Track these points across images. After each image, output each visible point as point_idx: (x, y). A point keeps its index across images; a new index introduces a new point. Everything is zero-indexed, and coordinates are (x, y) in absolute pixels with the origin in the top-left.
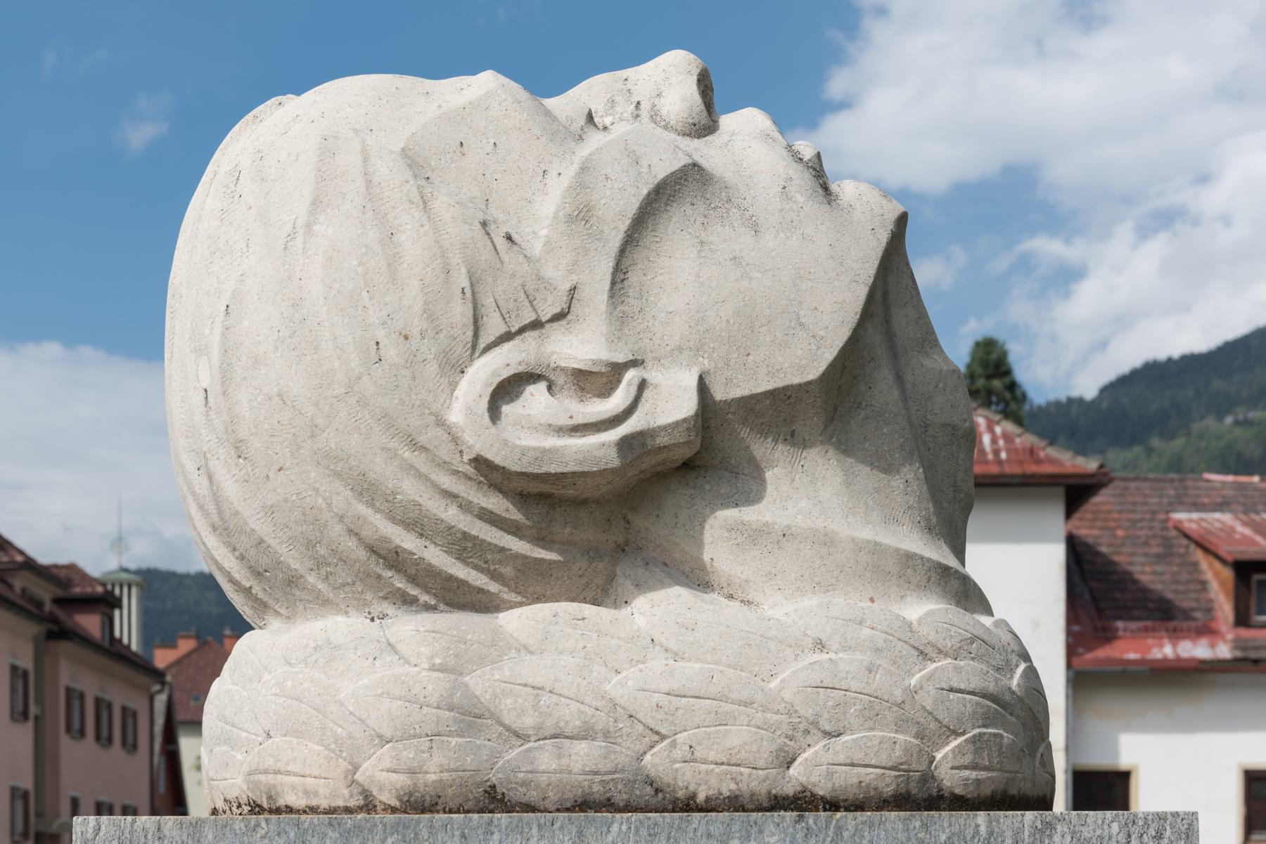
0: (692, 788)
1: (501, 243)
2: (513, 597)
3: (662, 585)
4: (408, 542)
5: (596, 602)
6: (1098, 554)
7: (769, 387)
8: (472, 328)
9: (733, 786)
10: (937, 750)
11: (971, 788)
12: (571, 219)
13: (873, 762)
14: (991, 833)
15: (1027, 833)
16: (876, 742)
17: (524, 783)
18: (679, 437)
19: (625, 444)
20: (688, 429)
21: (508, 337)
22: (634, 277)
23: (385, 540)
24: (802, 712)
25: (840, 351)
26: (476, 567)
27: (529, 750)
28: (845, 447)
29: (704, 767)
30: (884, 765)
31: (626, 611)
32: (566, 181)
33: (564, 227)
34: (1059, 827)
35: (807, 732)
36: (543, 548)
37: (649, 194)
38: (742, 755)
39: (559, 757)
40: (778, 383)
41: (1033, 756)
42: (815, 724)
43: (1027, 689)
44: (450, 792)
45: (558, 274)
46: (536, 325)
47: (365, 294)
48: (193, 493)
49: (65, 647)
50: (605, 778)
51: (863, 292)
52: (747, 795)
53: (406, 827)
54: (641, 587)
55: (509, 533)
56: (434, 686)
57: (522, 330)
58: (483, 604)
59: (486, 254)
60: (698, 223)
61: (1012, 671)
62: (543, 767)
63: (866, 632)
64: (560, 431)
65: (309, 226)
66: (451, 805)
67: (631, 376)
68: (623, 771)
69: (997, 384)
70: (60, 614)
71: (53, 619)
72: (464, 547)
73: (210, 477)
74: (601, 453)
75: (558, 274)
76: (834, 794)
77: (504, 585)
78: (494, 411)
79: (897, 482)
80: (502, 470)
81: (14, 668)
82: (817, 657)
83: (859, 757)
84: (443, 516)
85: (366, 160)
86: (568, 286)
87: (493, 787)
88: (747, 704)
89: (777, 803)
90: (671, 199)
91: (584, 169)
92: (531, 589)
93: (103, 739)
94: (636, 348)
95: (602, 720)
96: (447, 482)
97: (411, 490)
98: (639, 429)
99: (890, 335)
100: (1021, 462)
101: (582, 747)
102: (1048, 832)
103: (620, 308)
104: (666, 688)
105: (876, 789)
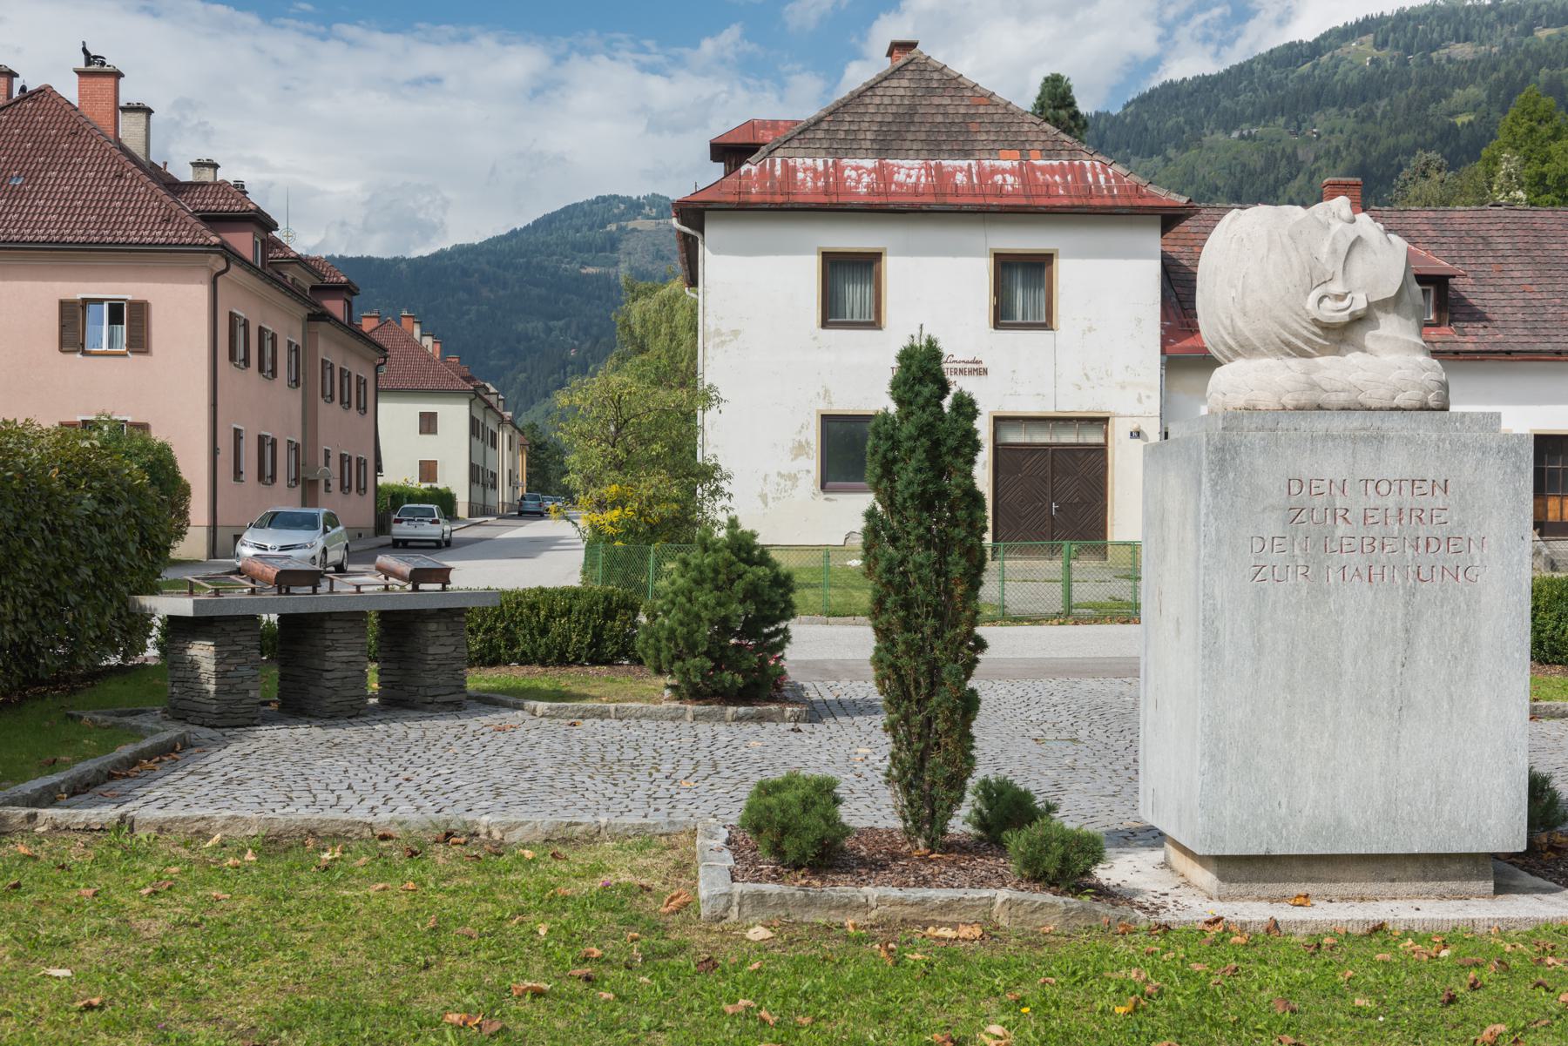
4: (1293, 340)
6: (1181, 265)
19: (1351, 314)
45: (1329, 268)
56: (1303, 378)
69: (1063, 113)
72: (1308, 341)
81: (290, 344)
89: (1392, 409)
93: (346, 404)
95: (1347, 387)
96: (1305, 324)
97: (1295, 326)
100: (1129, 197)
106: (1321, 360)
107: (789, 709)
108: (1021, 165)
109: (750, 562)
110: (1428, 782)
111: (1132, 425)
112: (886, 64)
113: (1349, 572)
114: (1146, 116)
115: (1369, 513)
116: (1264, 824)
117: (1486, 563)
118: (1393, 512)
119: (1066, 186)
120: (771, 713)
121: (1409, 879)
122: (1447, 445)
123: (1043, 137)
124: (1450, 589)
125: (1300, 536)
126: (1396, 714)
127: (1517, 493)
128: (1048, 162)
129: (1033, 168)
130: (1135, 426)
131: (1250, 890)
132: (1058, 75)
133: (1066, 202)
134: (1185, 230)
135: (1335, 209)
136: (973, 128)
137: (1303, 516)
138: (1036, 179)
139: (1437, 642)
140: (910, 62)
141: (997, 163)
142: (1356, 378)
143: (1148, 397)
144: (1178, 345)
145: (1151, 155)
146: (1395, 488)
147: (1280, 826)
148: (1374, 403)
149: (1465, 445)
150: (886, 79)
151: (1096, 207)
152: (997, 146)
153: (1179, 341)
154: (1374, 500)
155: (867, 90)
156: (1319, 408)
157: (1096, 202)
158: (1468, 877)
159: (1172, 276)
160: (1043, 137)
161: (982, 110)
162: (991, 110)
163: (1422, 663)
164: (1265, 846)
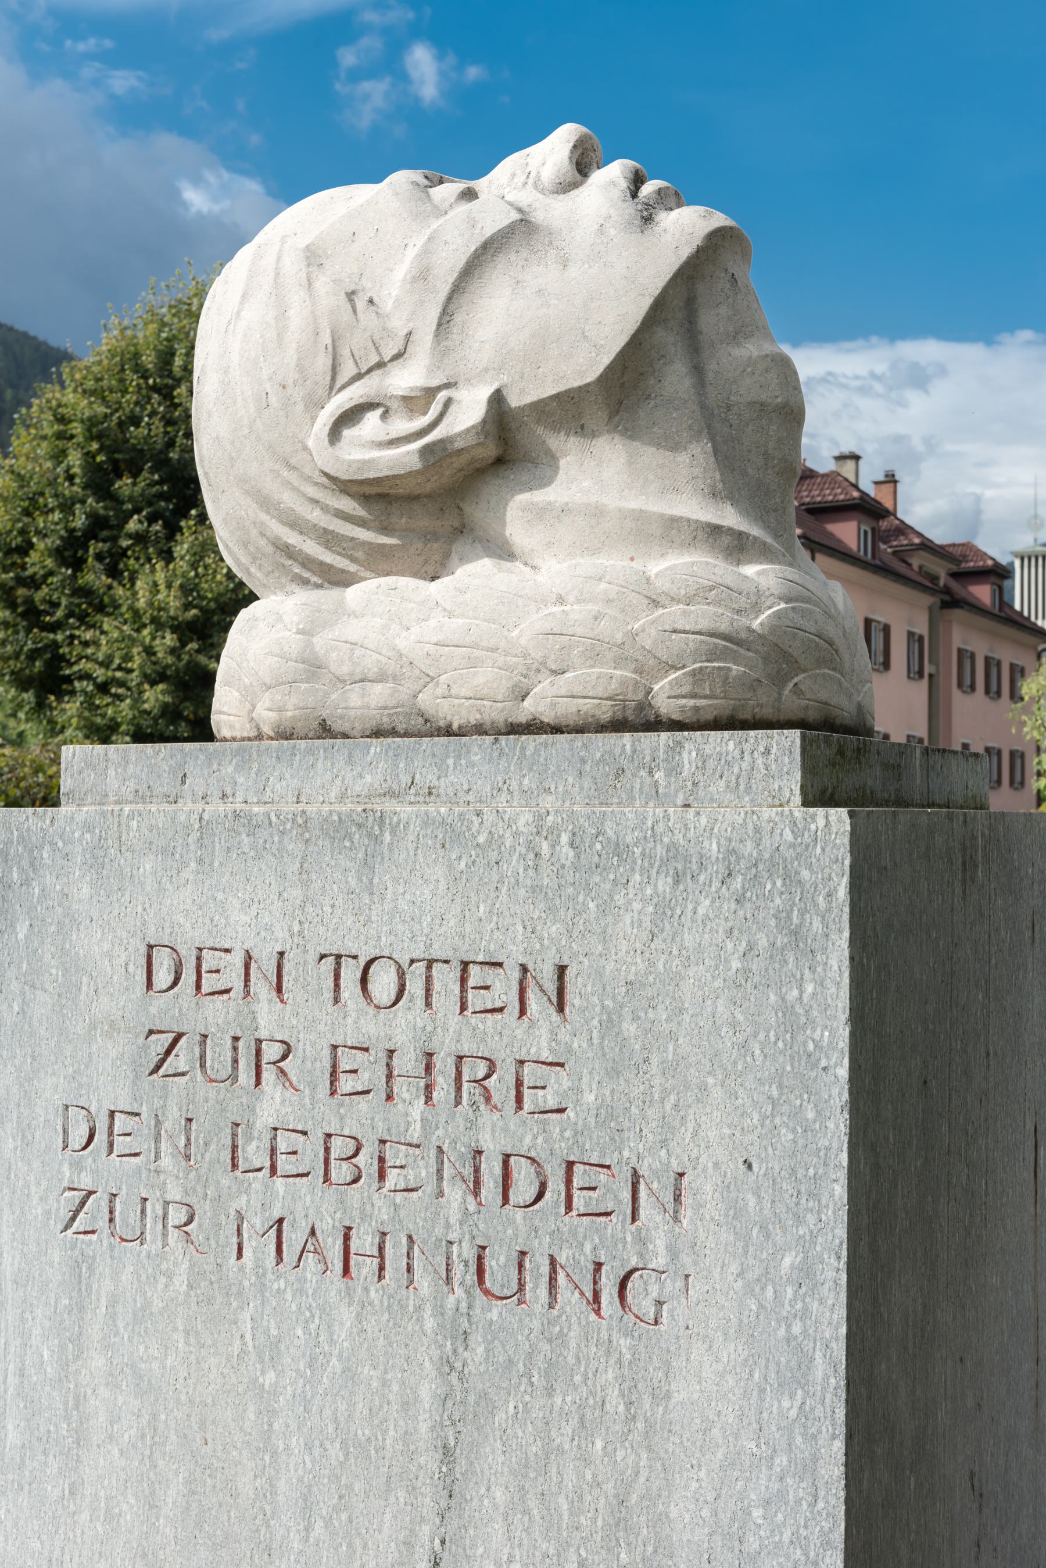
0: (448, 718)
2: (368, 574)
3: (478, 557)
4: (292, 538)
7: (554, 392)
8: (330, 374)
9: (478, 716)
10: (656, 683)
11: (689, 714)
12: (415, 280)
13: (590, 694)
14: (634, 751)
15: (662, 751)
16: (594, 677)
17: (341, 717)
18: (471, 440)
19: (426, 451)
20: (477, 433)
21: (359, 377)
22: (458, 318)
24: (533, 655)
25: (617, 355)
27: (345, 692)
28: (631, 433)
29: (457, 701)
30: (600, 696)
33: (409, 286)
34: (687, 745)
35: (538, 671)
36: (386, 535)
37: (476, 250)
38: (485, 691)
39: (363, 696)
40: (561, 388)
42: (544, 663)
44: (299, 724)
47: (262, 358)
49: (958, 613)
50: (391, 711)
52: (488, 723)
53: (244, 751)
55: (359, 526)
56: (294, 643)
57: (370, 371)
58: (341, 580)
60: (519, 266)
62: (352, 705)
66: (301, 734)
67: (442, 396)
68: (403, 706)
70: (954, 585)
71: (947, 590)
72: (328, 539)
74: (407, 459)
75: (399, 325)
76: (556, 721)
77: (361, 566)
79: (683, 458)
81: (911, 634)
83: (577, 690)
84: (309, 517)
86: (405, 332)
87: (324, 720)
88: (494, 650)
89: (515, 729)
90: (499, 250)
91: (430, 239)
92: (380, 567)
94: (452, 373)
95: (392, 667)
96: (311, 491)
97: (288, 499)
98: (439, 438)
101: (378, 688)
102: (678, 750)
103: (445, 343)
104: (434, 640)
105: (593, 716)
117: (686, 1260)
118: (407, 1062)
122: (566, 852)
124: (574, 1335)
137: (181, 1059)
139: (533, 1504)
148: (459, 714)
149: (619, 850)
156: (325, 731)
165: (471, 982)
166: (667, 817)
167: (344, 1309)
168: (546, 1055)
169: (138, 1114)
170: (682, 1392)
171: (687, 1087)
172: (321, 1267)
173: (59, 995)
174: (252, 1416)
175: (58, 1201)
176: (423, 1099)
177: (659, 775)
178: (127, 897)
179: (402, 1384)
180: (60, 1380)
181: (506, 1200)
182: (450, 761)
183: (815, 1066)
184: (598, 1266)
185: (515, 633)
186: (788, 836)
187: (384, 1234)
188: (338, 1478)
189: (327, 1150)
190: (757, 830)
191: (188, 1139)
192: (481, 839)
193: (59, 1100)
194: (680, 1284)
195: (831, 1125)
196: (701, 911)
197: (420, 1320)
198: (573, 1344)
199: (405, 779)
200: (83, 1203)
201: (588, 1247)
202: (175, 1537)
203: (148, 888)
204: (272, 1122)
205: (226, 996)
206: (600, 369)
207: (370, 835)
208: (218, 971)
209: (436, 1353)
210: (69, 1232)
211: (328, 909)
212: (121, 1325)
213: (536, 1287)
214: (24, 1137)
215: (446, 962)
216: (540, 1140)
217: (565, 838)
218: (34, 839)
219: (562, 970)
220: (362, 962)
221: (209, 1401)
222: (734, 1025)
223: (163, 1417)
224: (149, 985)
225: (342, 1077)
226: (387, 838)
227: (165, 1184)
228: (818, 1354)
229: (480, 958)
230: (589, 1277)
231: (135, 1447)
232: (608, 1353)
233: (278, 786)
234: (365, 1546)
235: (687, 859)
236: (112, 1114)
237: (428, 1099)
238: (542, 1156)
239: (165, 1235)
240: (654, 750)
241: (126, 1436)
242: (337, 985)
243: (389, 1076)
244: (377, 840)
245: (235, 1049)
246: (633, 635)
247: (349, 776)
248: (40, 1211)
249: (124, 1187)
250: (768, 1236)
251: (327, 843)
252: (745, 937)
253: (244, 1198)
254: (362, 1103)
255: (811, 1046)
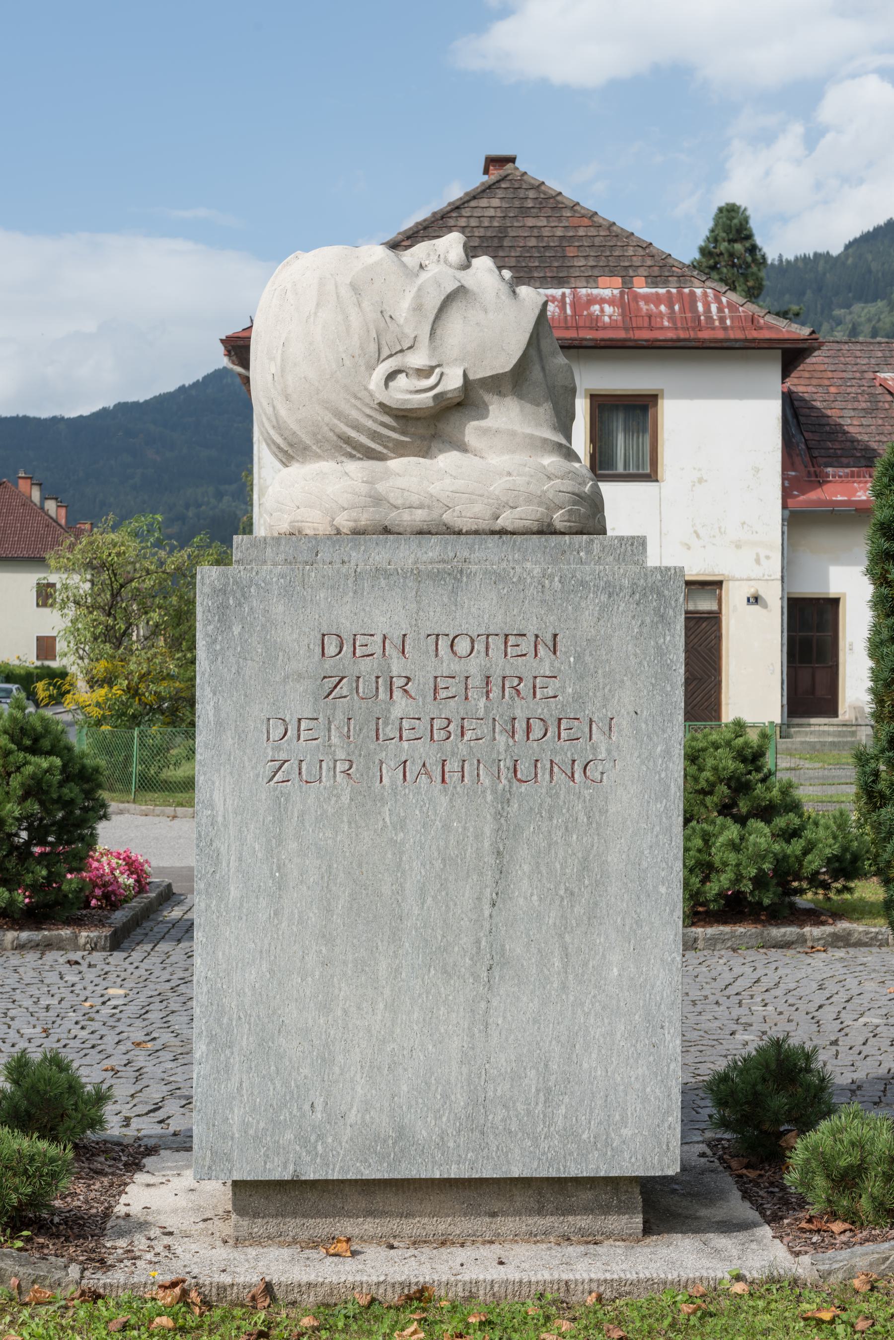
1: (388, 319)
2: (392, 455)
3: (449, 451)
4: (353, 434)
5: (423, 457)
6: (814, 408)
12: (414, 310)
17: (398, 525)
18: (456, 394)
19: (436, 397)
21: (391, 356)
22: (438, 332)
23: (345, 433)
26: (378, 444)
28: (521, 396)
31: (435, 460)
32: (412, 294)
35: (504, 506)
41: (594, 518)
42: (507, 503)
43: (592, 492)
45: (410, 331)
46: (402, 351)
48: (265, 414)
51: (528, 336)
54: (441, 451)
56: (364, 488)
57: (396, 353)
58: (380, 457)
59: (383, 325)
61: (586, 485)
63: (527, 469)
64: (411, 392)
65: (315, 313)
67: (437, 370)
69: (738, 247)
72: (374, 436)
73: (274, 408)
75: (410, 331)
78: (386, 385)
79: (541, 410)
80: (390, 407)
82: (508, 478)
83: (523, 516)
85: (336, 287)
86: (413, 336)
88: (482, 496)
89: (493, 533)
90: (453, 300)
91: (419, 289)
95: (427, 502)
96: (368, 411)
97: (354, 414)
99: (539, 351)
100: (743, 329)
101: (420, 511)
106: (395, 464)
107: (84, 934)
108: (622, 294)
109: (34, 750)
110: (532, 1074)
111: (749, 590)
112: (478, 179)
113: (413, 769)
114: (870, 257)
115: (441, 684)
116: (289, 1136)
117: (615, 754)
119: (672, 317)
120: (61, 939)
121: (518, 1213)
122: (557, 584)
123: (649, 262)
125: (340, 717)
126: (484, 975)
127: (660, 652)
128: (654, 290)
129: (636, 297)
130: (752, 591)
131: (283, 1228)
132: (734, 205)
133: (670, 335)
134: (811, 368)
135: (441, 250)
136: (570, 252)
137: (344, 688)
138: (639, 309)
139: (544, 870)
140: (504, 178)
141: (595, 291)
142: (440, 488)
143: (768, 557)
144: (802, 498)
145: (874, 300)
146: (479, 646)
147: (313, 1138)
148: (466, 524)
149: (583, 583)
150: (474, 198)
151: (704, 341)
152: (596, 272)
153: (803, 493)
154: (448, 664)
155: (452, 210)
156: (386, 531)
157: (705, 335)
158: (606, 1210)
159: (802, 420)
160: (649, 262)
161: (581, 232)
162: (592, 232)
163: (521, 901)
164: (291, 1168)
165: (510, 644)
166: (605, 569)
167: (442, 798)
168: (548, 673)
169: (316, 719)
170: (612, 809)
171: (615, 682)
172: (429, 780)
173: (264, 663)
174: (390, 856)
175: (264, 767)
176: (485, 697)
177: (582, 554)
178: (309, 611)
179: (475, 827)
180: (267, 858)
181: (528, 738)
182: (477, 547)
183: (670, 669)
184: (574, 761)
185: (492, 488)
186: (659, 577)
187: (464, 761)
188: (440, 877)
189: (432, 726)
190: (645, 575)
191: (349, 729)
192: (514, 580)
193: (264, 715)
194: (612, 764)
195: (677, 692)
196: (621, 609)
197: (485, 797)
198: (562, 796)
199: (451, 555)
200: (280, 767)
201: (569, 754)
202: (344, 923)
203: (322, 606)
204: (400, 716)
205: (371, 658)
206: (511, 366)
207: (455, 578)
208: (366, 645)
209: (492, 811)
210: (272, 783)
211: (432, 613)
212: (307, 825)
213: (544, 774)
214: (240, 737)
215: (497, 635)
216: (545, 711)
217: (556, 579)
218: (244, 582)
219: (555, 636)
220: (451, 637)
221: (364, 853)
222: (636, 655)
223: (335, 866)
224: (323, 654)
225: (441, 691)
226: (465, 579)
227: (335, 751)
228: (672, 784)
229: (515, 632)
230: (570, 767)
231: (317, 884)
232: (579, 798)
233: (377, 558)
234: (455, 904)
235: (614, 587)
236: (300, 720)
237: (488, 697)
238: (544, 716)
239: (335, 776)
240: (580, 543)
241: (312, 880)
242: (437, 649)
243: (466, 689)
244: (459, 581)
245: (377, 682)
246: (545, 492)
247: (419, 554)
248: (252, 774)
249: (308, 756)
250: (651, 740)
251: (431, 583)
252: (640, 619)
253: (384, 753)
254: (452, 702)
255: (669, 661)
